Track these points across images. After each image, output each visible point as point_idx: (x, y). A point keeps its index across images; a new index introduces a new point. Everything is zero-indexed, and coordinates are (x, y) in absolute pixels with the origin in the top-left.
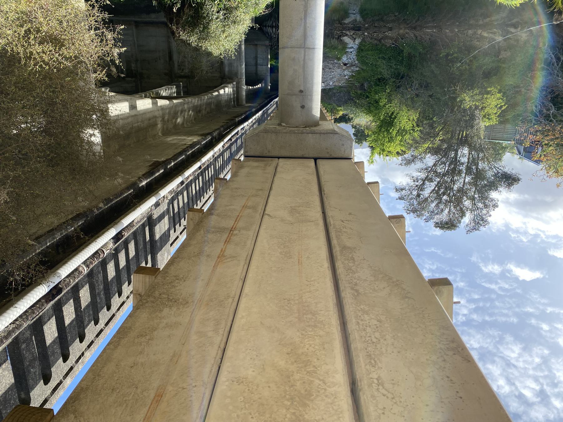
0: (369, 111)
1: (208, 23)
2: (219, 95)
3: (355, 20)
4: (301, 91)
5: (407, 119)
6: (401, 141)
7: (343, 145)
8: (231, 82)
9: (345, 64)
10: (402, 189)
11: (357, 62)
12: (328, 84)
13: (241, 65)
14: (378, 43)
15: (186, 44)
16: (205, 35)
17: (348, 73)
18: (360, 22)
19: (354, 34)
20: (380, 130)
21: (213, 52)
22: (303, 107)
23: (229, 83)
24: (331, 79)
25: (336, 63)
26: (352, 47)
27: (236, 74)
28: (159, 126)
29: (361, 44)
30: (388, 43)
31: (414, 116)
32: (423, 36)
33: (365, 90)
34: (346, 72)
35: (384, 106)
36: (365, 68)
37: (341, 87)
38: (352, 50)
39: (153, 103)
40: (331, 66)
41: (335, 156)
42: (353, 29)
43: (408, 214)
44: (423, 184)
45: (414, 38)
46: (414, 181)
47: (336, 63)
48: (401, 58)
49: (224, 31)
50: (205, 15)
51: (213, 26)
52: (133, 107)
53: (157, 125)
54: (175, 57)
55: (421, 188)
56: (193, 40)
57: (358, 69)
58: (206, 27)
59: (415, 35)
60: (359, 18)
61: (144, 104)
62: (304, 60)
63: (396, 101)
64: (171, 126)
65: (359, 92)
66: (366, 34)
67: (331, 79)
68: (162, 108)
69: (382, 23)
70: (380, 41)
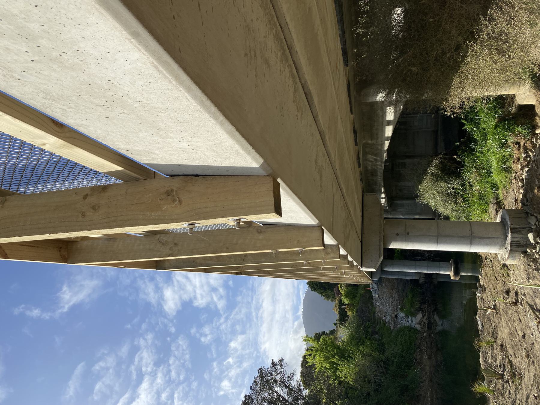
0: (352, 338)
1: (445, 181)
2: (381, 193)
3: (437, 325)
4: (408, 234)
5: (346, 372)
6: (325, 368)
7: (372, 261)
8: (388, 206)
9: (396, 316)
10: (281, 366)
11: (398, 327)
12: (377, 301)
13: (402, 215)
14: (417, 346)
15: (429, 164)
16: (437, 178)
17: (388, 319)
18: (436, 329)
19: (425, 323)
20: (335, 348)
21: (422, 185)
22: (397, 234)
23: (388, 203)
24: (382, 304)
25: (397, 307)
26: (412, 322)
27: (394, 210)
28: (370, 142)
29: (416, 330)
30: (417, 356)
31: (350, 379)
32: (423, 389)
33: (372, 336)
34: (388, 317)
35: (359, 351)
36: (393, 334)
37: (374, 313)
38: (410, 321)
39: (388, 137)
40: (394, 303)
41: (363, 256)
42: (429, 322)
43: (258, 370)
44: (286, 386)
45: (422, 380)
46: (289, 377)
47: (397, 307)
48: (403, 367)
49: (438, 193)
50: (451, 179)
51: (443, 184)
52: (389, 123)
53: (371, 140)
54: (408, 161)
55: (282, 383)
56: (432, 169)
57: (392, 328)
58: (442, 179)
59: (425, 380)
60: (439, 328)
61: (389, 131)
62: (430, 236)
63: (363, 361)
64: (367, 150)
65: (370, 330)
66: (425, 335)
67: (382, 304)
68: (383, 144)
69: (435, 349)
70: (419, 348)
